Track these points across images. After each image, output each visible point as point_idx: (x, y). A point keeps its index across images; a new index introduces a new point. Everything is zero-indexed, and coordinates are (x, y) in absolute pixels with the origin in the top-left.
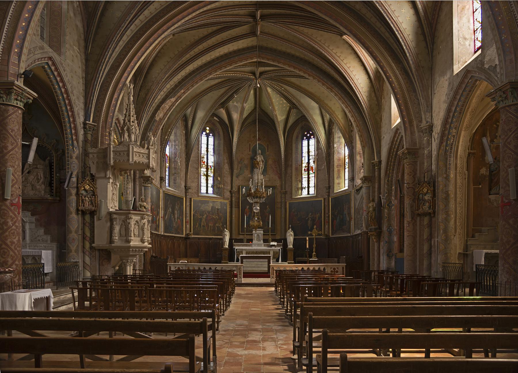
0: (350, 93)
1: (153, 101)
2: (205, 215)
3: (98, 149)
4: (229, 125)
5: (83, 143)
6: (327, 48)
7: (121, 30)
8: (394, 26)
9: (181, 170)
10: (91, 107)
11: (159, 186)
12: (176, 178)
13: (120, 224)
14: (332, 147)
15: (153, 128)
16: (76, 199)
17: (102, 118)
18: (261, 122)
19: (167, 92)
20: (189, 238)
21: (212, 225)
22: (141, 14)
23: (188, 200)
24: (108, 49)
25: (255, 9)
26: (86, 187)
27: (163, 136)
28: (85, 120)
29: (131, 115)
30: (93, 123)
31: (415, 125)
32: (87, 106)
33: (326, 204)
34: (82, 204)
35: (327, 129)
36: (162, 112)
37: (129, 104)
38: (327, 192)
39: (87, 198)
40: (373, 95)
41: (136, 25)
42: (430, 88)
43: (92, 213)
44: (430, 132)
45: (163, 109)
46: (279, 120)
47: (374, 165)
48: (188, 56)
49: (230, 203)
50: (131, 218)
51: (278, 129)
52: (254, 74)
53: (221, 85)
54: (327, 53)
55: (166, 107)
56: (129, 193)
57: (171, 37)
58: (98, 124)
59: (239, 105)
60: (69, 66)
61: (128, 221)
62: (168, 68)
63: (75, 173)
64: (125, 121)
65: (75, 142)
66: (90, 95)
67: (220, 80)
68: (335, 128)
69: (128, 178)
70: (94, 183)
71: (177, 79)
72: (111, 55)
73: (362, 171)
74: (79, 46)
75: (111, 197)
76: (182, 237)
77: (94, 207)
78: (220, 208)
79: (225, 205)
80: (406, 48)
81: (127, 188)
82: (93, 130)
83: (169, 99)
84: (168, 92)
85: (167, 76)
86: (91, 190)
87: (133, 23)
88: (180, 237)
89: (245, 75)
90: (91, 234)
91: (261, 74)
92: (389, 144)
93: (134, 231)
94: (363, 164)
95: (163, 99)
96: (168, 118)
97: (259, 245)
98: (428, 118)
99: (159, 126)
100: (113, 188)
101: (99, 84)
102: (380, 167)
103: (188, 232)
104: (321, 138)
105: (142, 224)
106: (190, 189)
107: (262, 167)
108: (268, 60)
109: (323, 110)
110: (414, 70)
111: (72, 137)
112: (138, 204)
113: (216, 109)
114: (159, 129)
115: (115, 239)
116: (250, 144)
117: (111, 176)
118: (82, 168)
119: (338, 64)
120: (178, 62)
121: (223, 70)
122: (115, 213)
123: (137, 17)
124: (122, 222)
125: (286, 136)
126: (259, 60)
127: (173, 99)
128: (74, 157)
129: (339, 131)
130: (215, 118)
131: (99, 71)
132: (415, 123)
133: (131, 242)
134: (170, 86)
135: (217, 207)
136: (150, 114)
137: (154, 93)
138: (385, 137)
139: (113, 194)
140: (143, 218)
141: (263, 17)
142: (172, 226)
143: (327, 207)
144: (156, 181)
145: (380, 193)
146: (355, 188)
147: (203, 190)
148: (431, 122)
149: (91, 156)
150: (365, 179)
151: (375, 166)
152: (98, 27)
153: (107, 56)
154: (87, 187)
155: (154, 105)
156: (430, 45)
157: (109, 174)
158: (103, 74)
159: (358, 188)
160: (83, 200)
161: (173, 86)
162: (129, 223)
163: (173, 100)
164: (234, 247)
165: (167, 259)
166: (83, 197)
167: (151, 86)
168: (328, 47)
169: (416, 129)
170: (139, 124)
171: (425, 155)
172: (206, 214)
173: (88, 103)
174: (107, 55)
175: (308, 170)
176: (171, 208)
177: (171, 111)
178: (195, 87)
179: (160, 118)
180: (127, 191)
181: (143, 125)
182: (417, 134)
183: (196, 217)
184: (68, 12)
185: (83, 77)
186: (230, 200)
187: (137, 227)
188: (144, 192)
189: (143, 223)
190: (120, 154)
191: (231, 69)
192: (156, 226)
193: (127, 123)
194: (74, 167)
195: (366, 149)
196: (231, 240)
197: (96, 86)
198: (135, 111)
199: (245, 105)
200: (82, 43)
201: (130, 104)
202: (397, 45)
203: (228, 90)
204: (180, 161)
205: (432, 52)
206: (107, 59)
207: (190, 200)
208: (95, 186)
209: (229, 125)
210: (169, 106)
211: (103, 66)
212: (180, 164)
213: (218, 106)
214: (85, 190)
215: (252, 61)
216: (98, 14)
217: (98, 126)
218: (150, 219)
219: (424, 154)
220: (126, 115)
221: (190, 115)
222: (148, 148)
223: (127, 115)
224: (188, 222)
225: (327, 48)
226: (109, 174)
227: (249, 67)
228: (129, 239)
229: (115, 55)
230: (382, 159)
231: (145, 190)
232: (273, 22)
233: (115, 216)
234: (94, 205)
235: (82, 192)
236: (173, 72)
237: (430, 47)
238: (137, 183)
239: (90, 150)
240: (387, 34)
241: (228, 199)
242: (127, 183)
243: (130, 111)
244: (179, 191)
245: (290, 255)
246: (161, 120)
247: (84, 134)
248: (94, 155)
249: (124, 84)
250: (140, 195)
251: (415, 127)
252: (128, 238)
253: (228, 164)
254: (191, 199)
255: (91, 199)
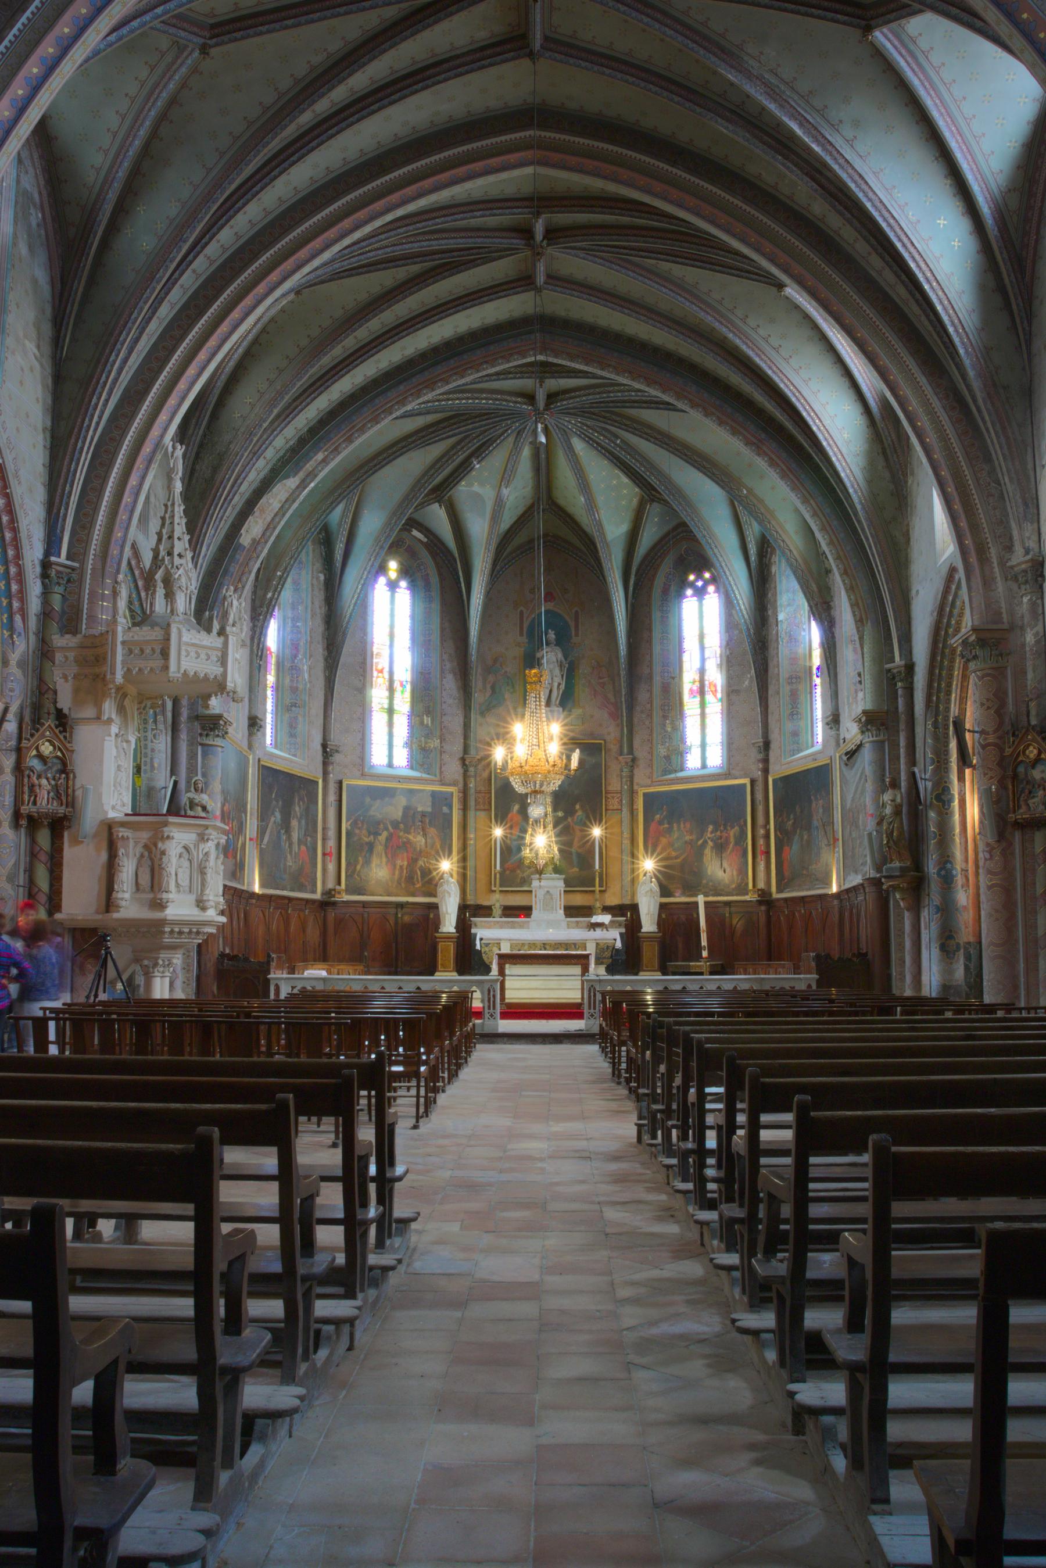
0: (812, 458)
1: (235, 488)
2: (385, 834)
3: (79, 636)
4: (457, 555)
5: (39, 620)
6: (741, 324)
7: (154, 289)
8: (918, 266)
9: (310, 695)
10: (65, 515)
11: (245, 744)
12: (296, 718)
13: (138, 855)
14: (772, 620)
15: (231, 569)
16: (13, 785)
17: (93, 547)
18: (554, 543)
19: (274, 462)
20: (334, 904)
21: (406, 863)
22: (211, 239)
23: (332, 787)
24: (118, 346)
25: (529, 213)
26: (42, 748)
27: (260, 593)
28: (47, 553)
29: (176, 537)
30: (69, 563)
31: (995, 560)
32: (55, 511)
33: (759, 796)
34: (30, 796)
35: (753, 565)
36: (260, 521)
37: (169, 504)
38: (759, 761)
39: (44, 782)
40: (881, 463)
41: (194, 271)
42: (1030, 450)
43: (59, 825)
44: (1036, 581)
45: (262, 511)
46: (610, 537)
47: (894, 678)
48: (337, 352)
49: (461, 795)
50: (168, 837)
51: (606, 565)
52: (531, 398)
53: (433, 432)
54: (740, 338)
55: (270, 504)
56: (160, 765)
57: (292, 296)
58: (83, 563)
59: (488, 493)
60: (11, 399)
61: (160, 845)
62: (279, 388)
63: (14, 708)
64: (158, 554)
65: (18, 618)
66: (62, 481)
67: (430, 418)
68: (780, 561)
69: (155, 722)
70: (65, 737)
71: (305, 422)
72: (125, 361)
73: (861, 695)
74: (39, 339)
75: (113, 776)
76: (313, 901)
77: (64, 807)
78: (429, 810)
79: (447, 800)
80: (956, 331)
81: (153, 750)
82: (69, 581)
83: (279, 481)
84: (279, 460)
85: (276, 411)
86: (57, 757)
87: (188, 266)
88: (307, 901)
89: (506, 401)
90: (51, 885)
91: (552, 397)
92: (933, 612)
93: (176, 875)
94: (859, 675)
95: (254, 491)
96: (278, 537)
97: (550, 924)
98: (1029, 538)
99: (251, 563)
100: (118, 752)
101: (89, 448)
102: (912, 683)
103: (330, 885)
104: (737, 592)
105: (201, 856)
106: (337, 751)
107: (559, 684)
108: (572, 358)
109: (740, 509)
110: (979, 396)
111: (10, 604)
112: (184, 799)
113: (422, 505)
114: (250, 572)
115: (122, 899)
116: (522, 613)
117: (114, 716)
118: (33, 692)
119: (774, 372)
120: (307, 371)
121: (438, 392)
122: (123, 824)
123: (198, 248)
124: (142, 850)
125: (631, 589)
126: (541, 358)
127: (292, 480)
128: (13, 663)
129: (789, 572)
130: (415, 533)
131: (91, 408)
132: (993, 553)
133: (166, 907)
134: (284, 441)
135: (420, 809)
136: (224, 527)
137: (237, 465)
138: (921, 592)
139: (119, 768)
140: (202, 838)
141: (553, 234)
142: (282, 866)
143: (760, 808)
144: (238, 730)
145: (912, 762)
146: (842, 745)
147: (378, 757)
148: (1037, 550)
149: (59, 657)
150: (870, 720)
151: (897, 679)
152: (92, 281)
153: (112, 366)
154: (47, 749)
155: (238, 501)
156: (1022, 323)
157: (109, 708)
158: (100, 417)
159: (851, 747)
160: (32, 787)
161: (291, 443)
162: (163, 853)
163: (292, 483)
164: (473, 931)
165: (268, 963)
166: (35, 778)
167: (230, 443)
168: (744, 320)
169: (996, 570)
170: (195, 559)
171: (1028, 649)
172: (386, 829)
173: (56, 504)
174: (114, 362)
175: (702, 692)
176: (281, 812)
177: (288, 515)
178: (357, 443)
179: (254, 540)
180: (152, 759)
181: (204, 561)
182: (1000, 586)
183: (355, 839)
184: (15, 244)
185: (44, 430)
186: (461, 785)
187: (187, 864)
188: (203, 762)
189: (205, 851)
190: (142, 651)
191: (471, 383)
192: (236, 864)
193: (163, 560)
194: (12, 690)
195: (868, 629)
196: (463, 908)
197: (81, 453)
198: (186, 524)
199: (505, 491)
200: (47, 329)
201: (173, 504)
202: (930, 321)
203: (453, 447)
204: (310, 668)
205: (1029, 342)
206: (113, 374)
207: (337, 785)
208: (68, 745)
209: (457, 555)
210: (280, 501)
211: (92, 416)
212: (310, 676)
213: (427, 495)
214: (40, 756)
215: (524, 361)
216: (92, 244)
217: (82, 569)
218: (223, 841)
219: (1023, 645)
220: (160, 535)
221: (340, 525)
222: (222, 632)
223: (165, 537)
224: (330, 854)
225: (741, 324)
226: (109, 708)
227: (515, 378)
228: (161, 899)
229: (135, 361)
230: (914, 660)
231: (205, 755)
232: (584, 249)
233: (122, 832)
234: (64, 801)
235: (31, 764)
236: (294, 400)
237: (1024, 329)
238: (183, 736)
239: (59, 641)
240: (902, 291)
241: (454, 784)
242: (154, 736)
243: (172, 523)
244: (304, 759)
245: (650, 953)
246: (256, 543)
247: (43, 593)
248: (67, 654)
249: (158, 445)
250: (192, 770)
251: (995, 565)
252: (159, 896)
253: (455, 674)
254: (340, 783)
255: (56, 785)
